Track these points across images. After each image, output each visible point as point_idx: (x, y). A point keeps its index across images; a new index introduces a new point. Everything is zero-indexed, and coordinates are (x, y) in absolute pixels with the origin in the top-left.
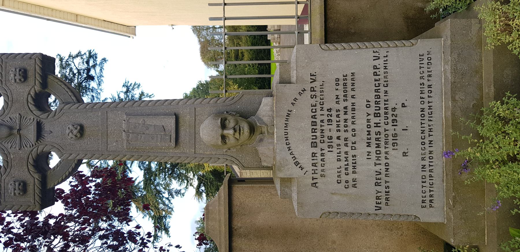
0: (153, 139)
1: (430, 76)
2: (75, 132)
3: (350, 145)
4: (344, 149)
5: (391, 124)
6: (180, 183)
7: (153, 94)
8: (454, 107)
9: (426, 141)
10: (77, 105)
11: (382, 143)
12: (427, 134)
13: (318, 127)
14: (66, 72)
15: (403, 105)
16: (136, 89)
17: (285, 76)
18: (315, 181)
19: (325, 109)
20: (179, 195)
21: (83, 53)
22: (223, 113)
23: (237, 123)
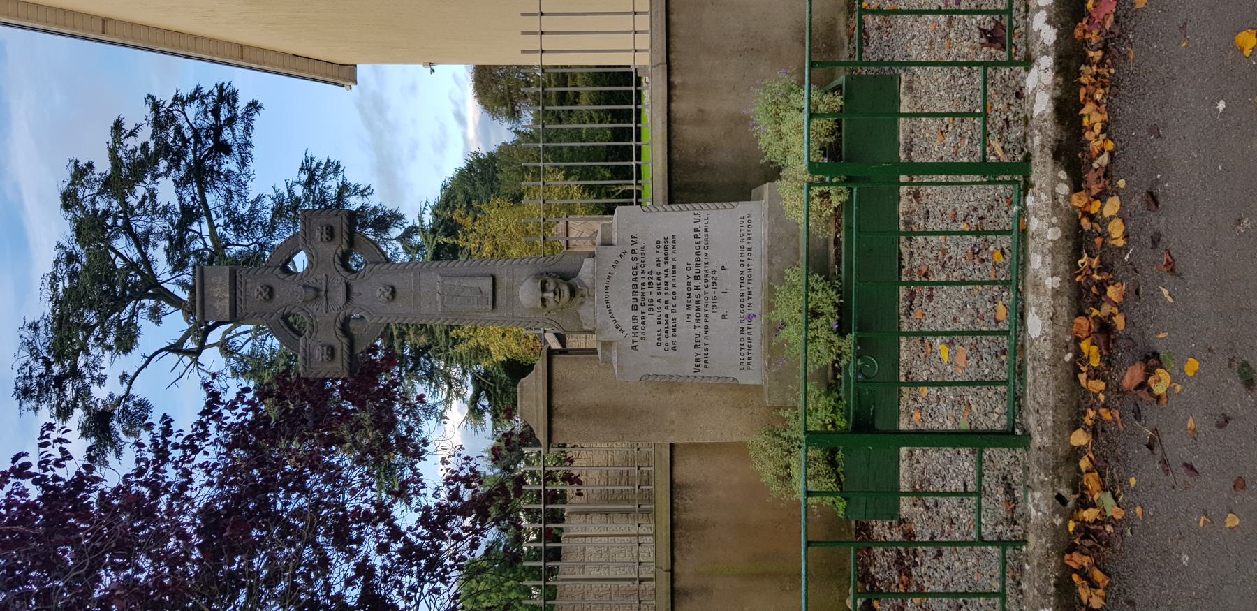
0: (469, 301)
1: (749, 239)
2: (387, 294)
3: (670, 307)
4: (664, 312)
5: (711, 287)
6: (432, 390)
7: (369, 188)
8: (770, 270)
9: (746, 304)
10: (387, 265)
11: (702, 306)
12: (746, 297)
13: (639, 290)
14: (168, 134)
15: (723, 268)
16: (331, 176)
17: (606, 237)
18: (635, 344)
19: (646, 272)
20: (433, 416)
21: (205, 92)
22: (542, 274)
23: (557, 285)
